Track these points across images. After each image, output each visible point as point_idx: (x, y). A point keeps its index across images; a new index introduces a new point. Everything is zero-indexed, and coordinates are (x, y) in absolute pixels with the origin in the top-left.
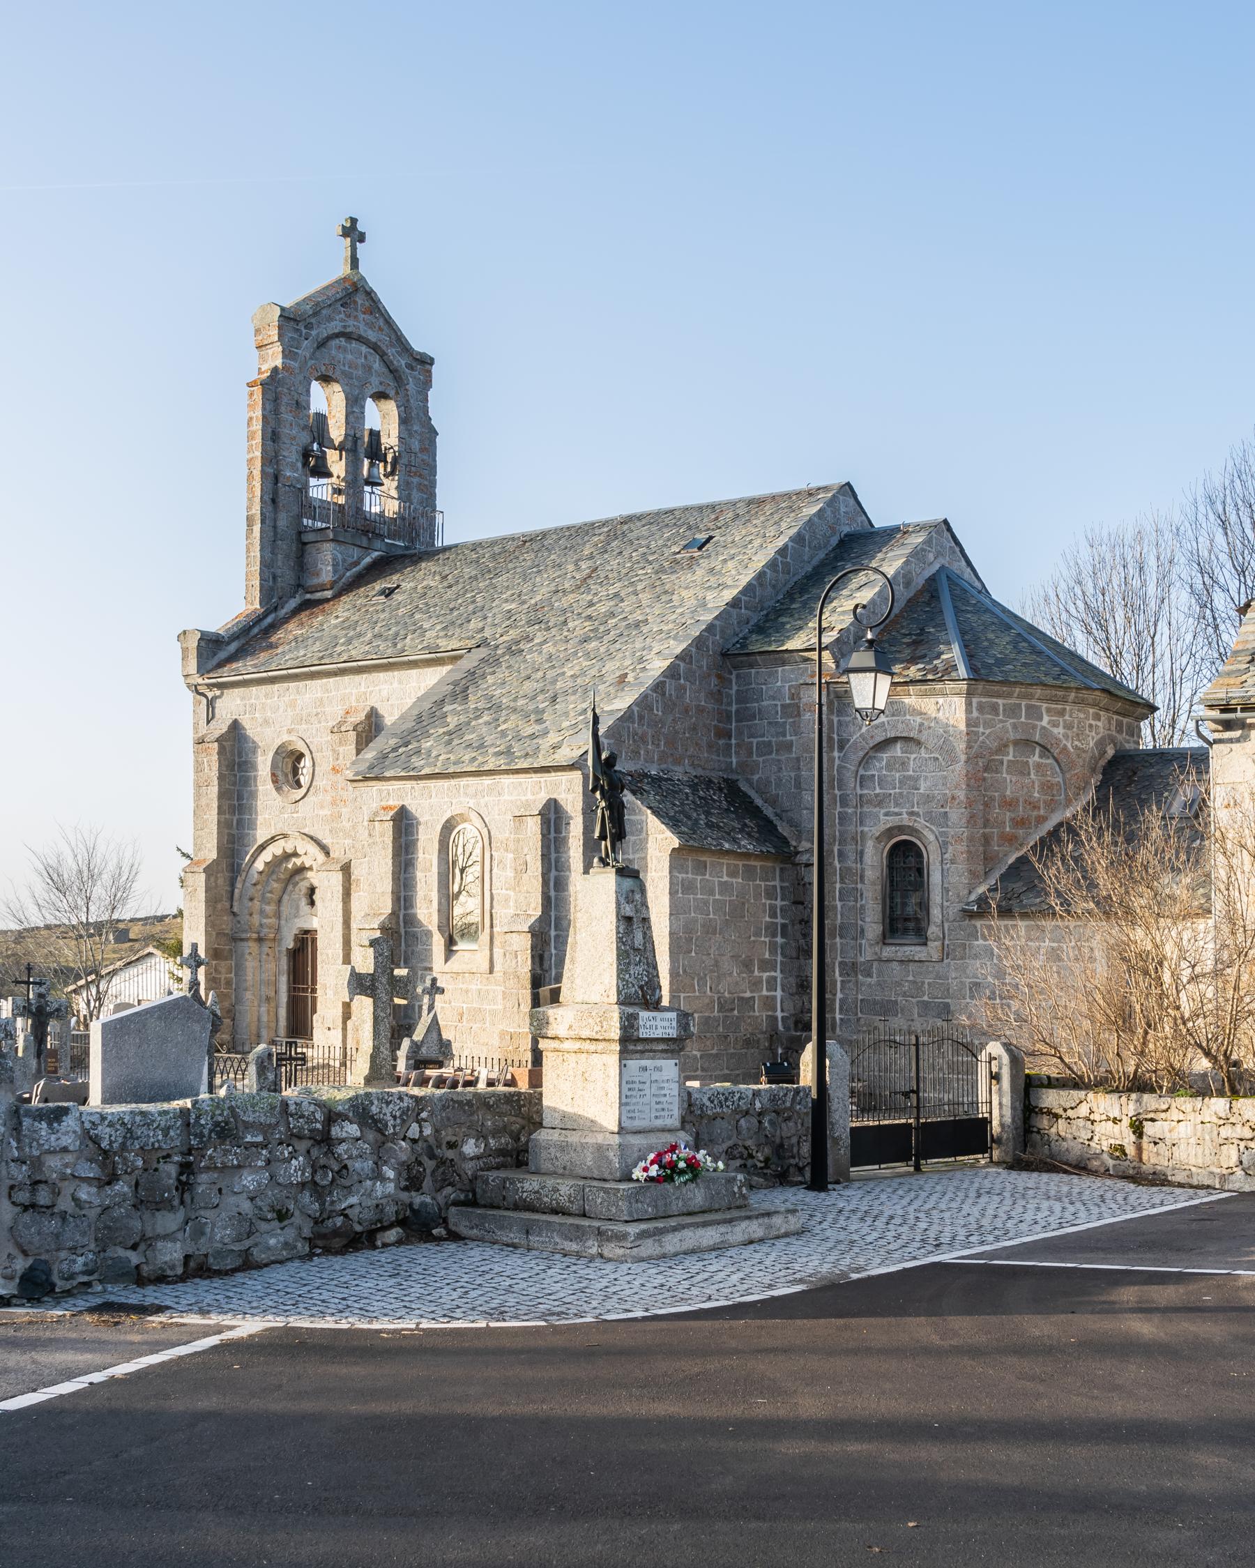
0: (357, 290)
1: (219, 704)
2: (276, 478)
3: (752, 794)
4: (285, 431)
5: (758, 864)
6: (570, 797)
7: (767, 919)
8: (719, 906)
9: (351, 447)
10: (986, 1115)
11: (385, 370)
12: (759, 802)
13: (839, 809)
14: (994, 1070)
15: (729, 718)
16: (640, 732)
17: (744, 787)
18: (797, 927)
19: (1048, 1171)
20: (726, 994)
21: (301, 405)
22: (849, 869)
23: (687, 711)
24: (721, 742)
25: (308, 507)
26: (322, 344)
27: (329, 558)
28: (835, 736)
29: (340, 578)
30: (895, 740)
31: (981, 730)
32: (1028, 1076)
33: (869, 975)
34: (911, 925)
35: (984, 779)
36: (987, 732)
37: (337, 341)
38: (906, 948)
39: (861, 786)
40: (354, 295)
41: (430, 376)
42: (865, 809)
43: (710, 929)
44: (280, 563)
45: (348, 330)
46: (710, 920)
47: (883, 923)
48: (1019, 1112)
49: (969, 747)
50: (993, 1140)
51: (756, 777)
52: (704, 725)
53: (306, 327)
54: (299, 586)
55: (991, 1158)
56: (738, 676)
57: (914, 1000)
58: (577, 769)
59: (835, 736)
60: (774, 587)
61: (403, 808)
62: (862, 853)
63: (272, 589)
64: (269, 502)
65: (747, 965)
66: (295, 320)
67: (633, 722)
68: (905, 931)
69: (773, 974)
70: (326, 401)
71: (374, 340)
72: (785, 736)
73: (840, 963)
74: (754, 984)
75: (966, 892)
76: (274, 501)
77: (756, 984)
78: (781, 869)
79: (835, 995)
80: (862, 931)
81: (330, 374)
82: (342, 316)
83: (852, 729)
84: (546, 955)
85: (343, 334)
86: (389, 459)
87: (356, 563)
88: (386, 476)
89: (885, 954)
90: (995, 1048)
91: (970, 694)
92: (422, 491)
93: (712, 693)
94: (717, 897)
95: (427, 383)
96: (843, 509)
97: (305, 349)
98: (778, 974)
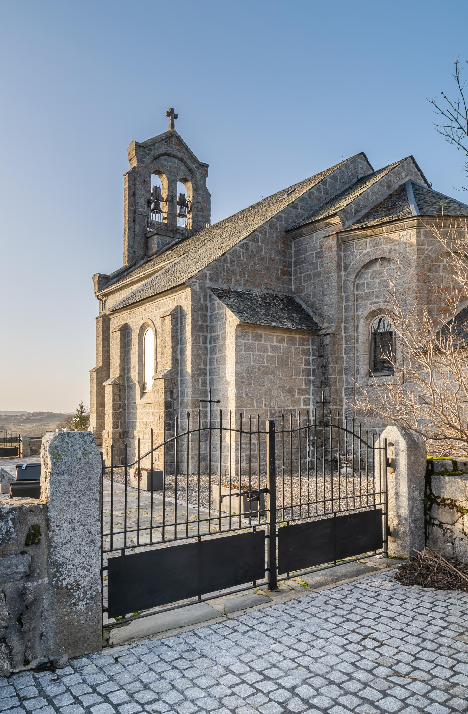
0: (172, 136)
1: (107, 303)
2: (135, 211)
3: (302, 303)
4: (138, 192)
5: (298, 336)
6: (186, 303)
7: (304, 366)
8: (271, 359)
9: (171, 199)
10: (382, 506)
11: (187, 170)
12: (304, 306)
13: (344, 304)
14: (391, 456)
15: (290, 265)
16: (231, 269)
17: (297, 300)
18: (321, 370)
19: (447, 587)
20: (276, 408)
21: (147, 183)
22: (350, 336)
23: (263, 260)
24: (285, 277)
25: (148, 223)
26: (156, 158)
27: (156, 242)
28: (343, 264)
29: (160, 250)
30: (376, 260)
31: (426, 247)
32: (430, 462)
34: (385, 365)
35: (429, 276)
36: (430, 248)
37: (164, 157)
38: (382, 378)
39: (357, 290)
40: (172, 137)
41: (207, 172)
42: (359, 302)
44: (136, 246)
46: (265, 366)
47: (370, 365)
48: (419, 503)
49: (419, 257)
50: (388, 533)
51: (303, 294)
52: (274, 268)
53: (148, 150)
54: (146, 255)
55: (386, 552)
56: (295, 243)
59: (343, 264)
60: (318, 200)
62: (357, 327)
63: (134, 257)
64: (132, 221)
65: (291, 392)
67: (227, 263)
68: (383, 369)
69: (307, 396)
70: (159, 182)
72: (317, 269)
73: (345, 389)
74: (295, 402)
76: (134, 221)
77: (297, 402)
78: (313, 339)
79: (342, 406)
80: (358, 370)
81: (161, 170)
82: (166, 146)
83: (351, 258)
84: (175, 391)
85: (165, 152)
86: (189, 206)
88: (188, 213)
89: (370, 382)
90: (392, 433)
91: (419, 226)
92: (203, 218)
93: (279, 252)
94: (269, 354)
95: (206, 175)
96: (360, 166)
97: (148, 159)
98: (311, 397)
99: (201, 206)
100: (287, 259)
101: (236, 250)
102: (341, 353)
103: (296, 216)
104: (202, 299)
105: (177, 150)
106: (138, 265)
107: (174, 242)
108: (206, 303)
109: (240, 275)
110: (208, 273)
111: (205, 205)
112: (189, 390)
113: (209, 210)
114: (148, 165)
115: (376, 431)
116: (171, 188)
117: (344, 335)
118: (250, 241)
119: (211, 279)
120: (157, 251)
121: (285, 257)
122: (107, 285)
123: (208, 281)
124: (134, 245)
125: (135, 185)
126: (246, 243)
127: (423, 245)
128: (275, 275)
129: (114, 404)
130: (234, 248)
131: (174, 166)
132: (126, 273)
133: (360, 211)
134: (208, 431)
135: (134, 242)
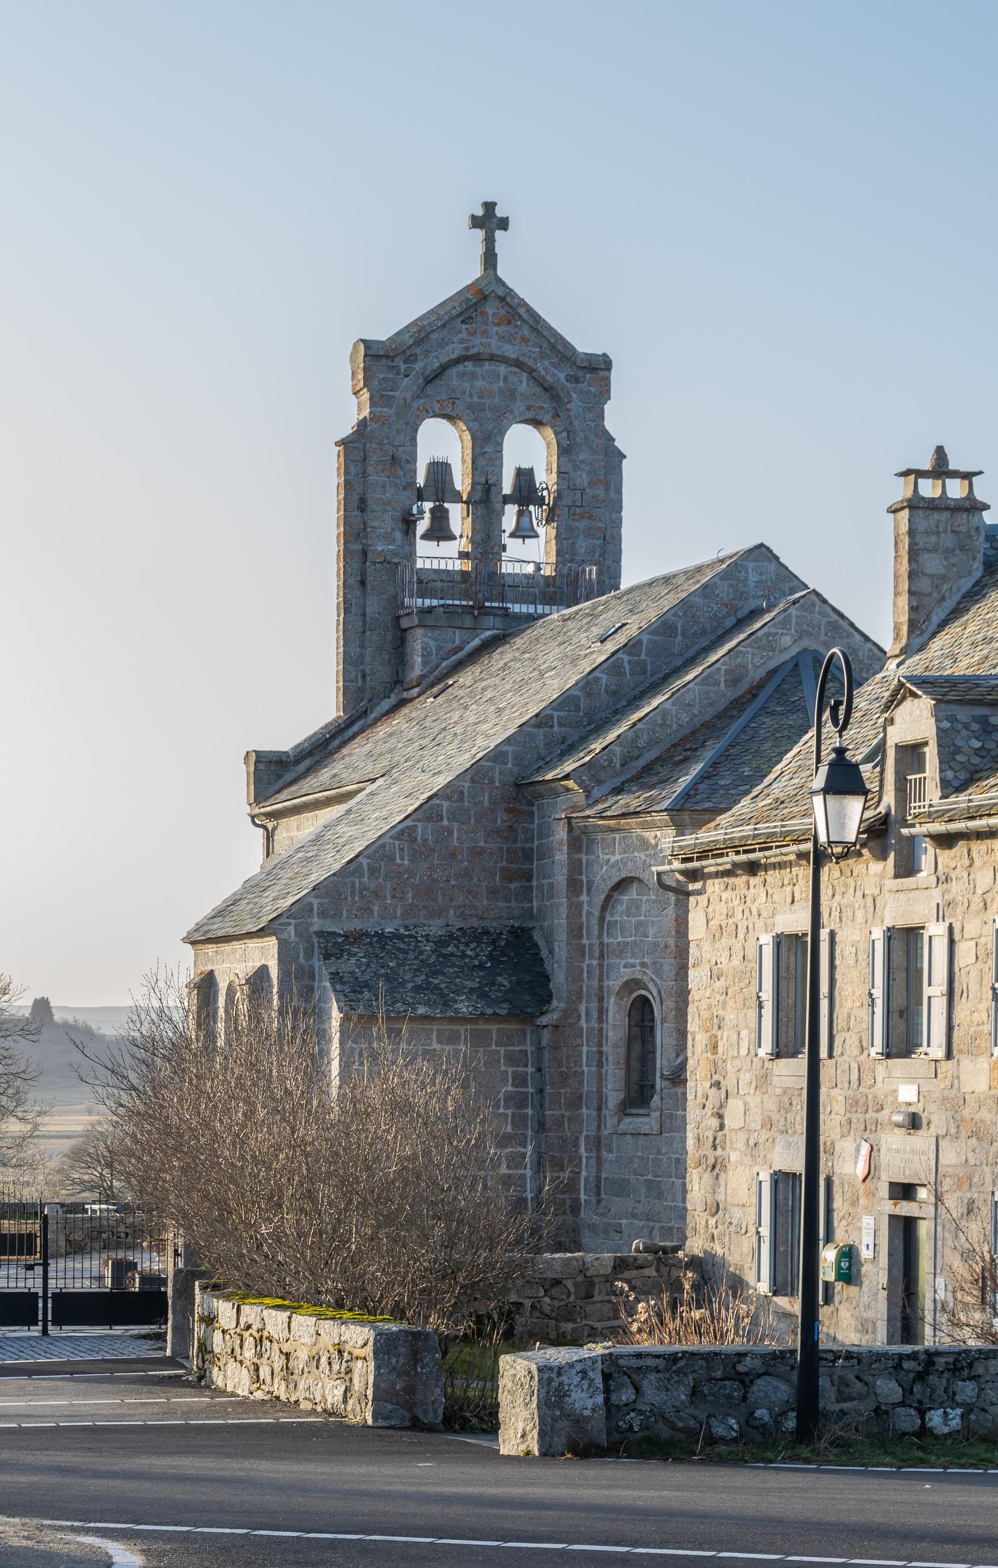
2: (365, 553)
4: (374, 497)
7: (510, 1088)
11: (538, 390)
13: (587, 962)
16: (372, 886)
23: (453, 855)
29: (431, 672)
33: (610, 1151)
37: (460, 367)
40: (488, 303)
45: (472, 352)
53: (406, 361)
57: (642, 1179)
58: (270, 935)
63: (362, 690)
66: (388, 357)
67: (361, 876)
71: (513, 356)
75: (674, 1054)
76: (363, 583)
78: (532, 1031)
79: (579, 1173)
82: (464, 335)
83: (596, 868)
87: (456, 651)
93: (498, 832)
95: (604, 393)
99: (589, 504)
100: (519, 845)
101: (383, 846)
102: (578, 1063)
103: (547, 744)
104: (302, 955)
105: (502, 338)
106: (373, 716)
107: (476, 642)
108: (311, 962)
109: (393, 897)
110: (315, 902)
111: (600, 492)
113: (617, 506)
114: (407, 405)
115: (620, 1224)
116: (482, 462)
117: (585, 1026)
118: (419, 820)
119: (322, 915)
120: (423, 677)
121: (515, 841)
122: (281, 783)
123: (316, 919)
124: (362, 656)
125: (364, 474)
126: (408, 828)
128: (484, 884)
130: (378, 844)
131: (495, 387)
132: (336, 743)
133: (638, 758)
135: (362, 646)
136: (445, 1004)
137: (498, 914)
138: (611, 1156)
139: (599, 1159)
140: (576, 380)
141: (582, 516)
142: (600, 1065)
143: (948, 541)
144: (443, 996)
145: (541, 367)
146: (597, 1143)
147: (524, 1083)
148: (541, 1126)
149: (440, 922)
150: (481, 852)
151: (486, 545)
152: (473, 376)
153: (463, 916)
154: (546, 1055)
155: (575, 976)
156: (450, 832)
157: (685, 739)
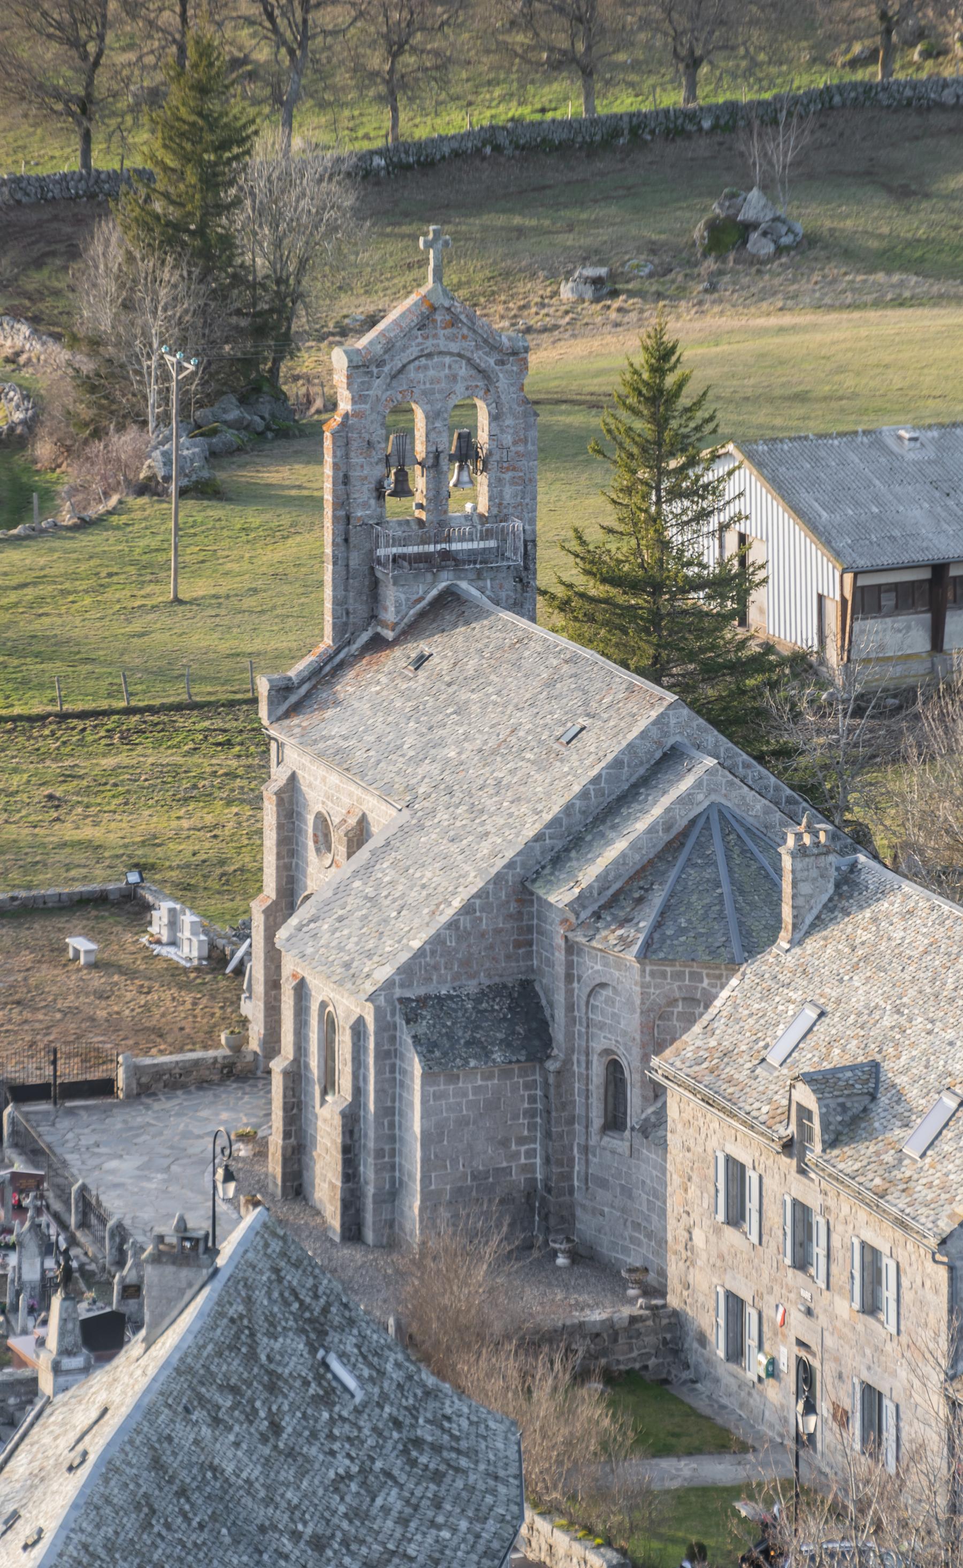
2: (348, 518)
4: (354, 474)
11: (473, 372)
43: (462, 1122)
49: (643, 1003)
61: (303, 979)
63: (346, 624)
76: (346, 540)
82: (420, 340)
93: (510, 916)
102: (572, 1094)
105: (447, 338)
112: (371, 1134)
119: (402, 986)
124: (346, 597)
125: (347, 456)
127: (649, 987)
129: (285, 1103)
131: (442, 374)
134: (392, 1194)
135: (346, 590)
136: (487, 1056)
137: (510, 973)
138: (596, 1160)
139: (587, 1161)
140: (501, 363)
141: (508, 469)
142: (587, 1098)
143: (814, 873)
144: (484, 1048)
145: (476, 356)
146: (585, 1149)
147: (535, 1101)
148: (548, 1135)
149: (474, 982)
150: (501, 930)
151: (438, 497)
152: (426, 368)
153: (489, 976)
154: (552, 1090)
155: (570, 1036)
156: (481, 919)
157: (637, 873)
